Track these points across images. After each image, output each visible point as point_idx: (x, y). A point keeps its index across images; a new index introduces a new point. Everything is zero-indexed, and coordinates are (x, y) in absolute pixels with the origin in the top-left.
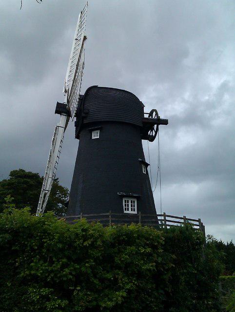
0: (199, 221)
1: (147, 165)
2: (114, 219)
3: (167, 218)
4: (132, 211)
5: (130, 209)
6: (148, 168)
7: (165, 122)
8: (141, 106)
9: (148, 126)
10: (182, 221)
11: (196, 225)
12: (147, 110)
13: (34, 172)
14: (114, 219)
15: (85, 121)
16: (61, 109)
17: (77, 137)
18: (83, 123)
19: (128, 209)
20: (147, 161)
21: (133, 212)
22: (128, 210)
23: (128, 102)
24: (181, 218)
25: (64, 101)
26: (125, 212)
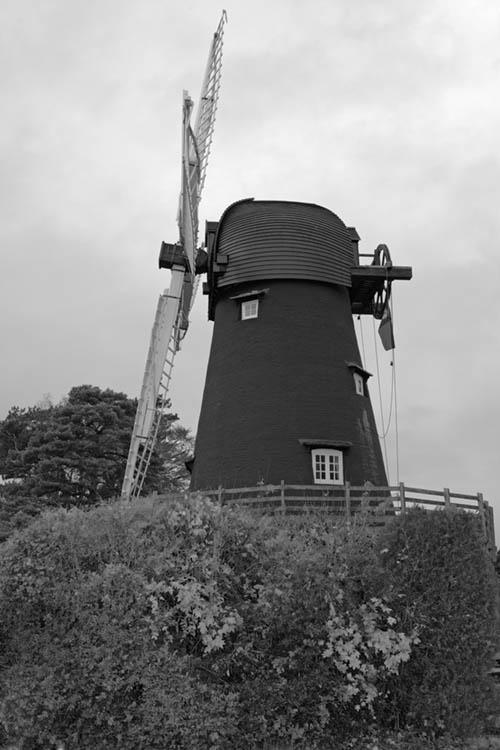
0: (478, 498)
1: (366, 376)
2: (340, 499)
3: (408, 495)
4: (332, 478)
5: (328, 476)
6: (370, 381)
7: (405, 274)
8: (352, 237)
9: (369, 287)
10: (441, 499)
11: (470, 507)
12: (366, 247)
13: (117, 390)
14: (340, 499)
15: (222, 283)
16: (170, 257)
17: (211, 317)
18: (216, 284)
19: (324, 474)
20: (367, 367)
21: (335, 482)
22: (324, 477)
23: (317, 227)
24: (473, 498)
25: (174, 239)
26: (317, 481)
